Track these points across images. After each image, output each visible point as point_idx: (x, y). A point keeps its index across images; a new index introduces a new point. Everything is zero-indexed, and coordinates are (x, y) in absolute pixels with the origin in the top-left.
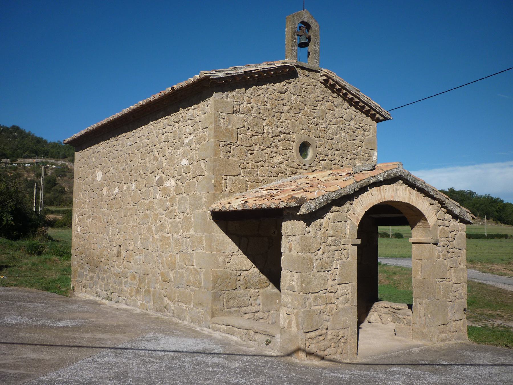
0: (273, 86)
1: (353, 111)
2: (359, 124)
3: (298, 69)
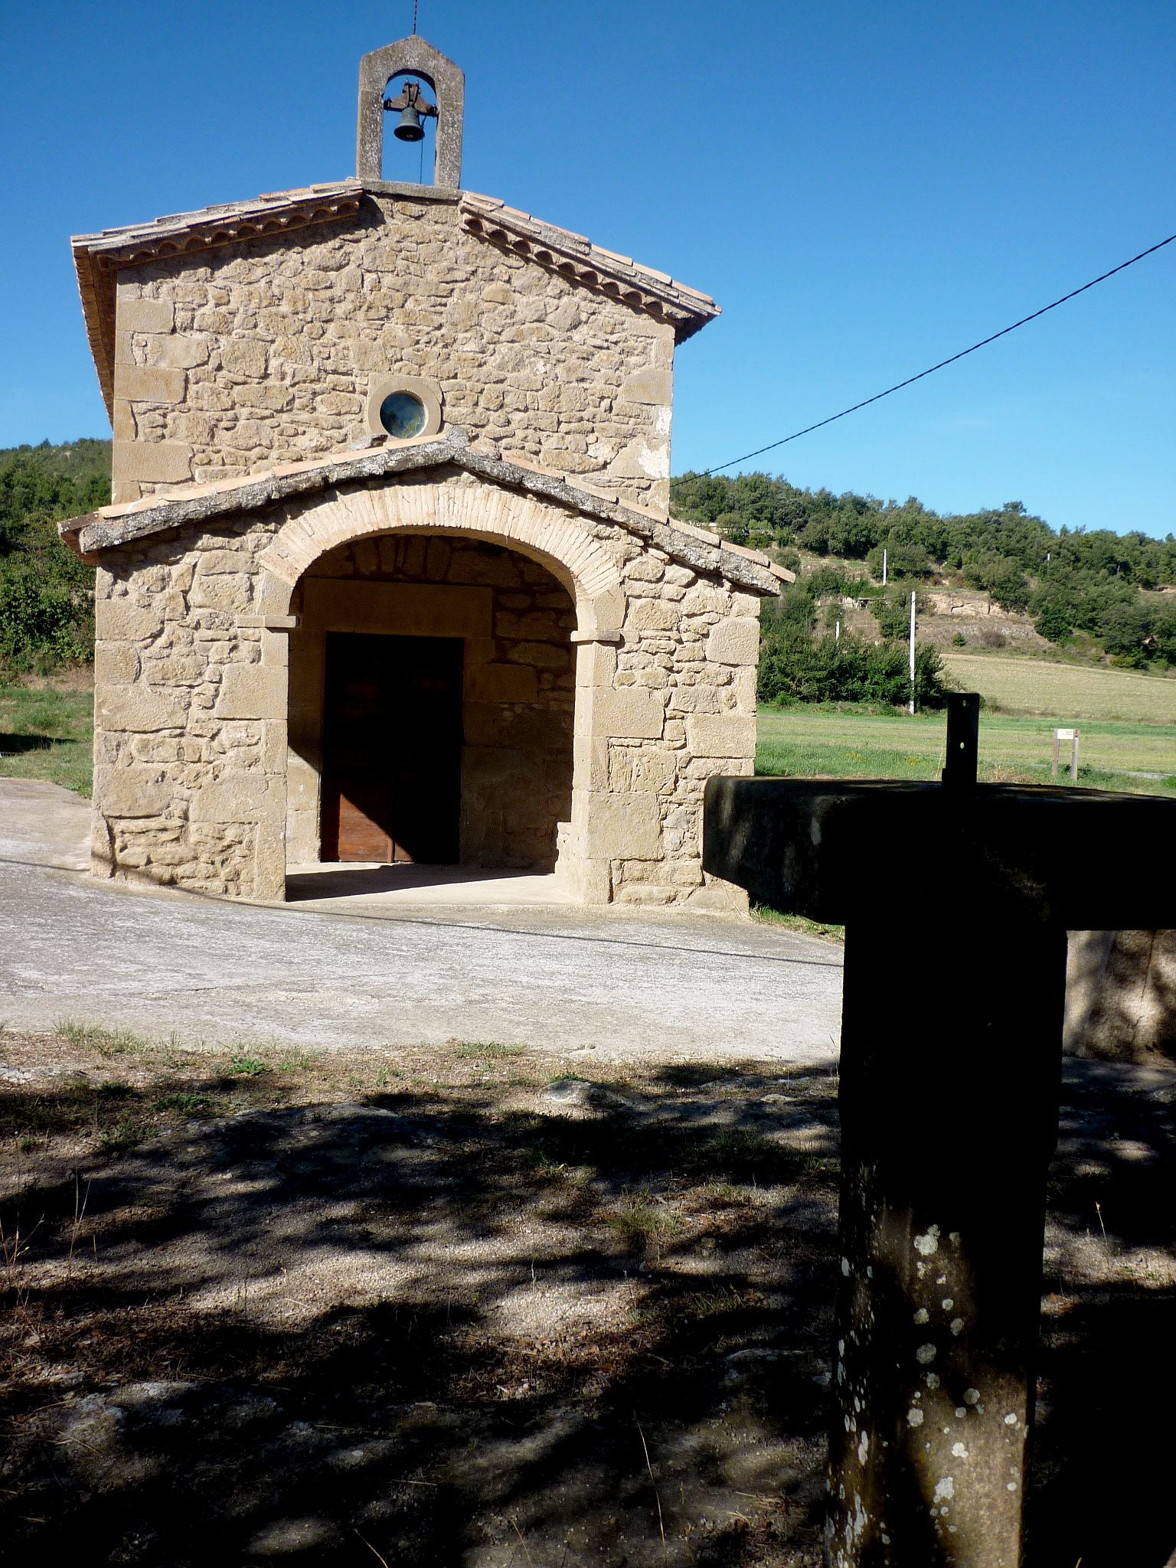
1: (585, 299)
3: (381, 203)
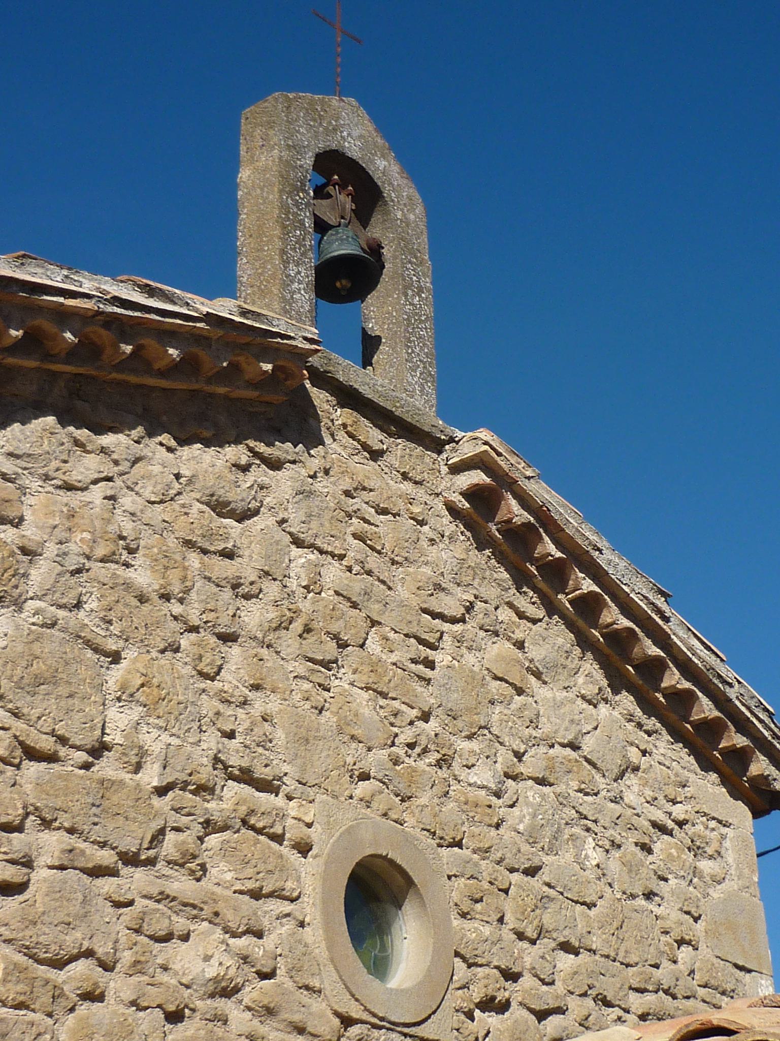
0: (170, 450)
1: (630, 718)
2: (669, 807)
